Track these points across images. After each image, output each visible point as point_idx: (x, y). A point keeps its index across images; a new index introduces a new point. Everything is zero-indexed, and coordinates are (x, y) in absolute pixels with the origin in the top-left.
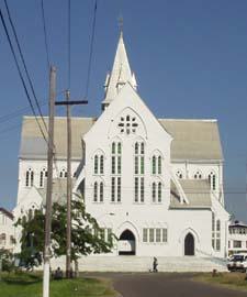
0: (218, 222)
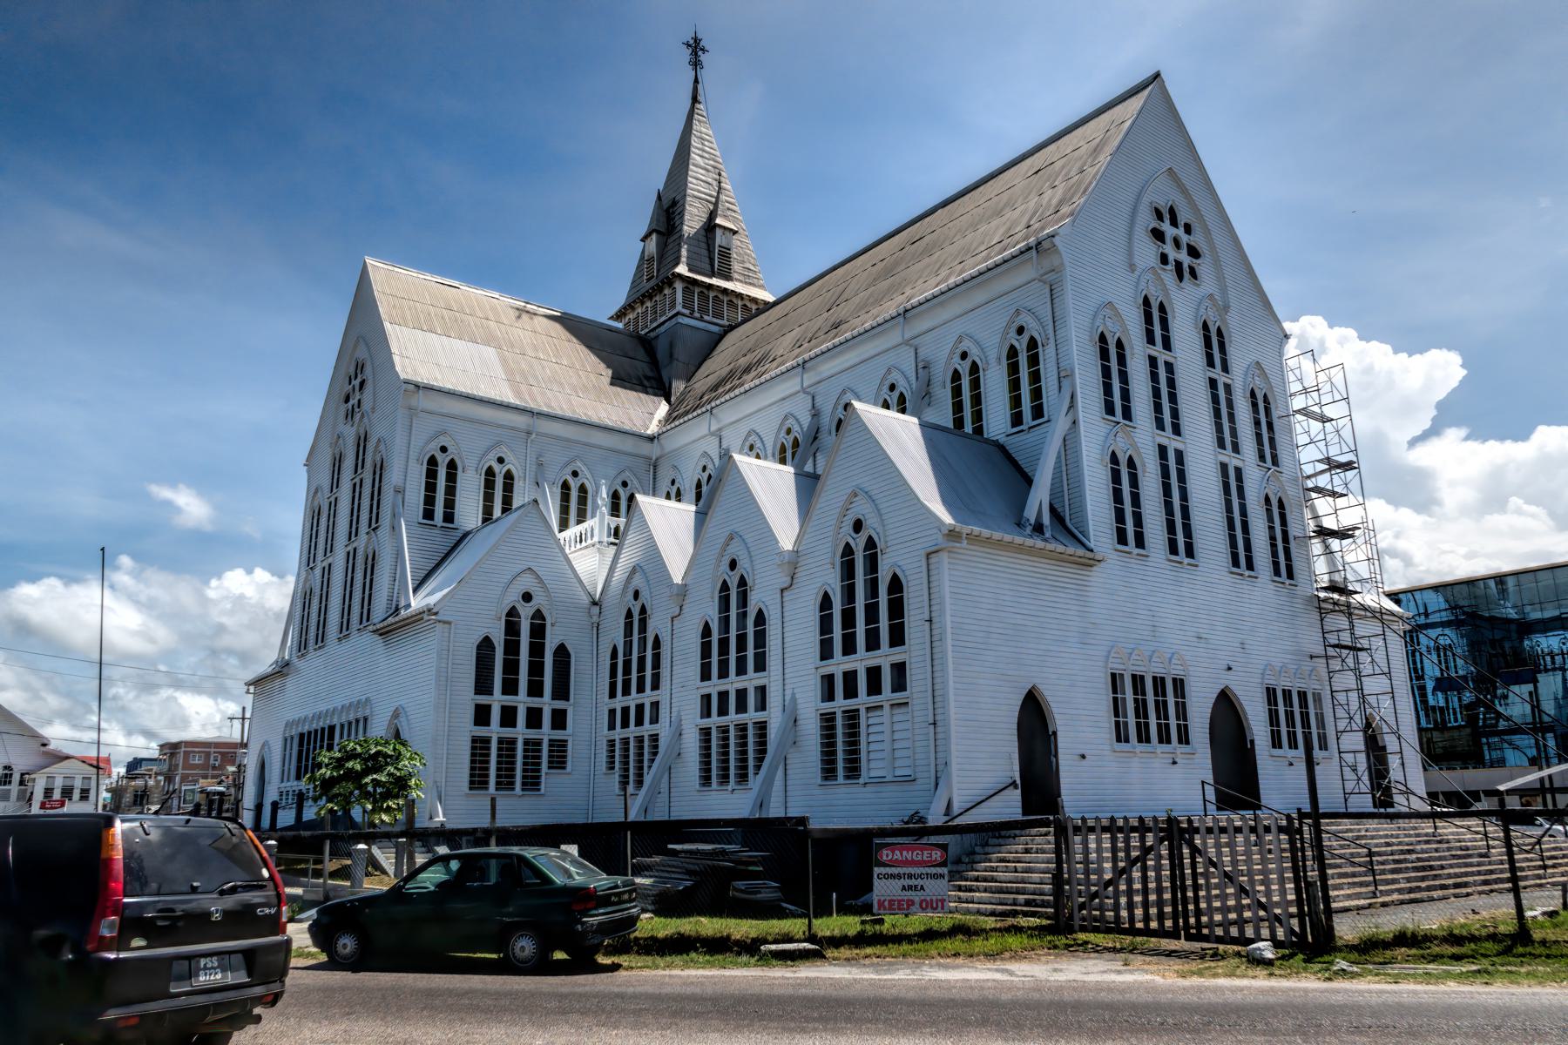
0: (562, 653)
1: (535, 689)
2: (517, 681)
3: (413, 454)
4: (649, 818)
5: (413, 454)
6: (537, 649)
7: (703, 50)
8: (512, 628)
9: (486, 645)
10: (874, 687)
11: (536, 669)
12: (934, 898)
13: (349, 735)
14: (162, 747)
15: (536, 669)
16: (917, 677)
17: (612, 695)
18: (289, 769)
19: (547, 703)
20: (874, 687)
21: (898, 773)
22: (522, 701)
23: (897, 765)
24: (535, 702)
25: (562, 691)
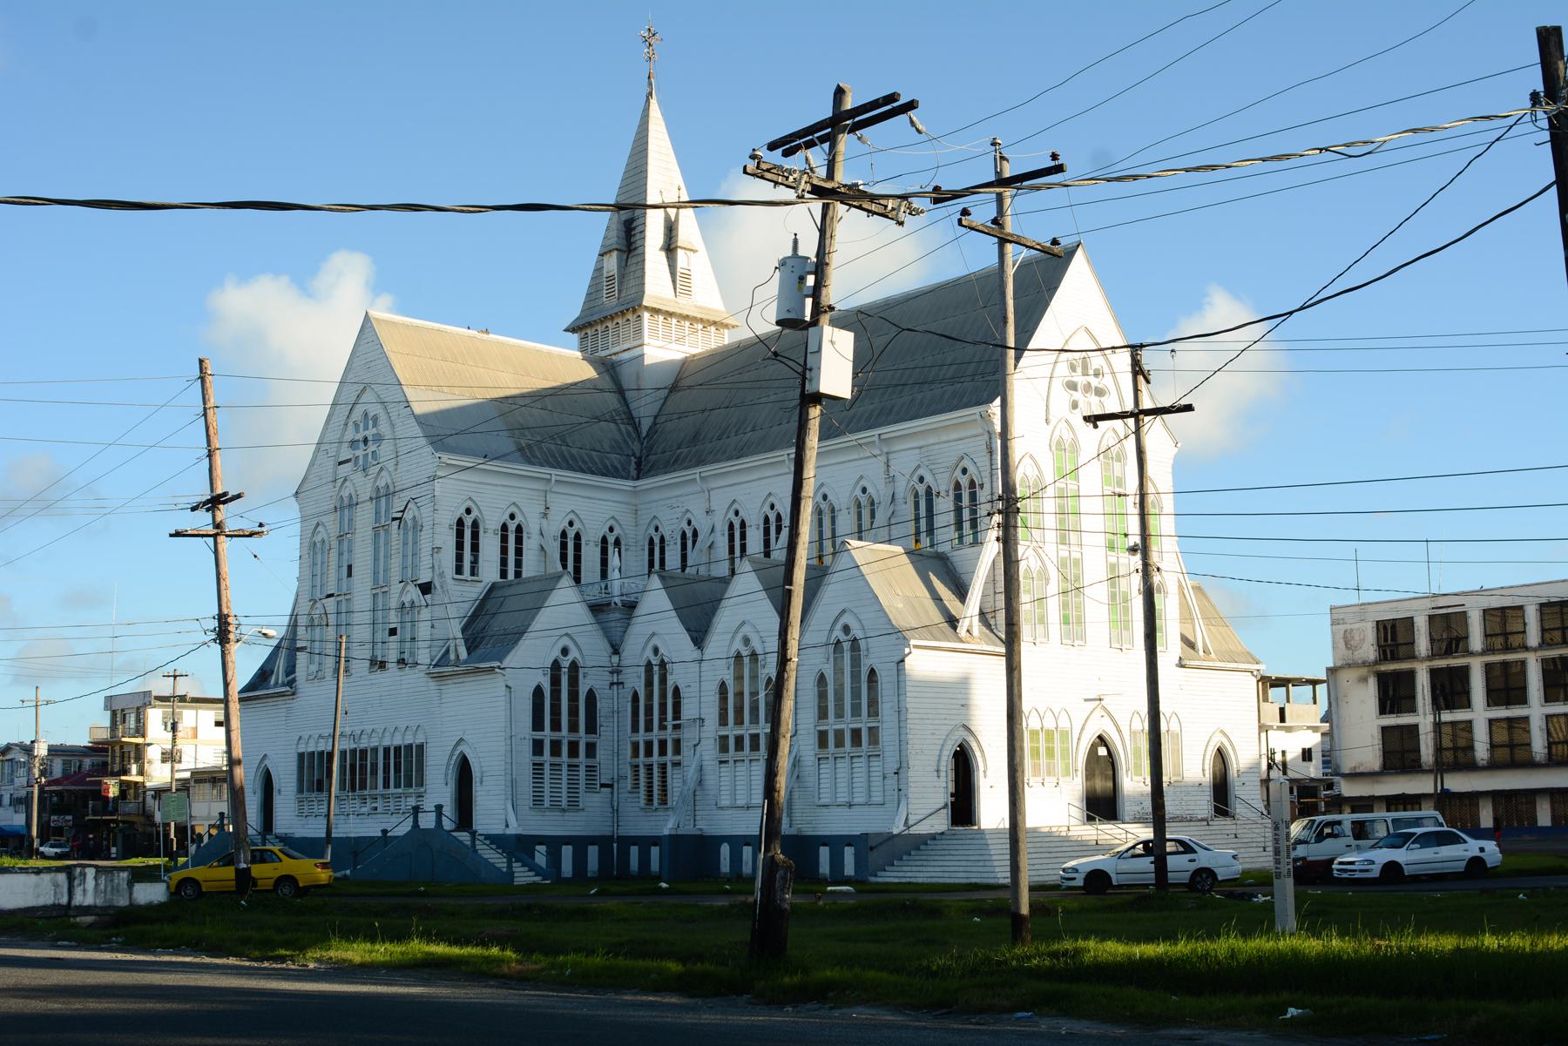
1: (556, 726)
2: (652, 705)
3: (401, 674)
4: (680, 833)
5: (401, 674)
6: (573, 696)
7: (1055, 242)
8: (555, 681)
9: (538, 692)
10: (839, 743)
11: (573, 712)
12: (392, 790)
13: (663, 719)
14: (435, 806)
15: (573, 712)
16: (887, 736)
17: (635, 729)
18: (944, 855)
19: (582, 737)
20: (839, 743)
21: (838, 800)
22: (656, 735)
23: (838, 796)
24: (556, 735)
25: (591, 728)
